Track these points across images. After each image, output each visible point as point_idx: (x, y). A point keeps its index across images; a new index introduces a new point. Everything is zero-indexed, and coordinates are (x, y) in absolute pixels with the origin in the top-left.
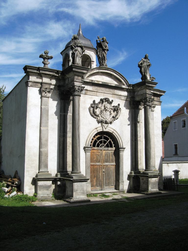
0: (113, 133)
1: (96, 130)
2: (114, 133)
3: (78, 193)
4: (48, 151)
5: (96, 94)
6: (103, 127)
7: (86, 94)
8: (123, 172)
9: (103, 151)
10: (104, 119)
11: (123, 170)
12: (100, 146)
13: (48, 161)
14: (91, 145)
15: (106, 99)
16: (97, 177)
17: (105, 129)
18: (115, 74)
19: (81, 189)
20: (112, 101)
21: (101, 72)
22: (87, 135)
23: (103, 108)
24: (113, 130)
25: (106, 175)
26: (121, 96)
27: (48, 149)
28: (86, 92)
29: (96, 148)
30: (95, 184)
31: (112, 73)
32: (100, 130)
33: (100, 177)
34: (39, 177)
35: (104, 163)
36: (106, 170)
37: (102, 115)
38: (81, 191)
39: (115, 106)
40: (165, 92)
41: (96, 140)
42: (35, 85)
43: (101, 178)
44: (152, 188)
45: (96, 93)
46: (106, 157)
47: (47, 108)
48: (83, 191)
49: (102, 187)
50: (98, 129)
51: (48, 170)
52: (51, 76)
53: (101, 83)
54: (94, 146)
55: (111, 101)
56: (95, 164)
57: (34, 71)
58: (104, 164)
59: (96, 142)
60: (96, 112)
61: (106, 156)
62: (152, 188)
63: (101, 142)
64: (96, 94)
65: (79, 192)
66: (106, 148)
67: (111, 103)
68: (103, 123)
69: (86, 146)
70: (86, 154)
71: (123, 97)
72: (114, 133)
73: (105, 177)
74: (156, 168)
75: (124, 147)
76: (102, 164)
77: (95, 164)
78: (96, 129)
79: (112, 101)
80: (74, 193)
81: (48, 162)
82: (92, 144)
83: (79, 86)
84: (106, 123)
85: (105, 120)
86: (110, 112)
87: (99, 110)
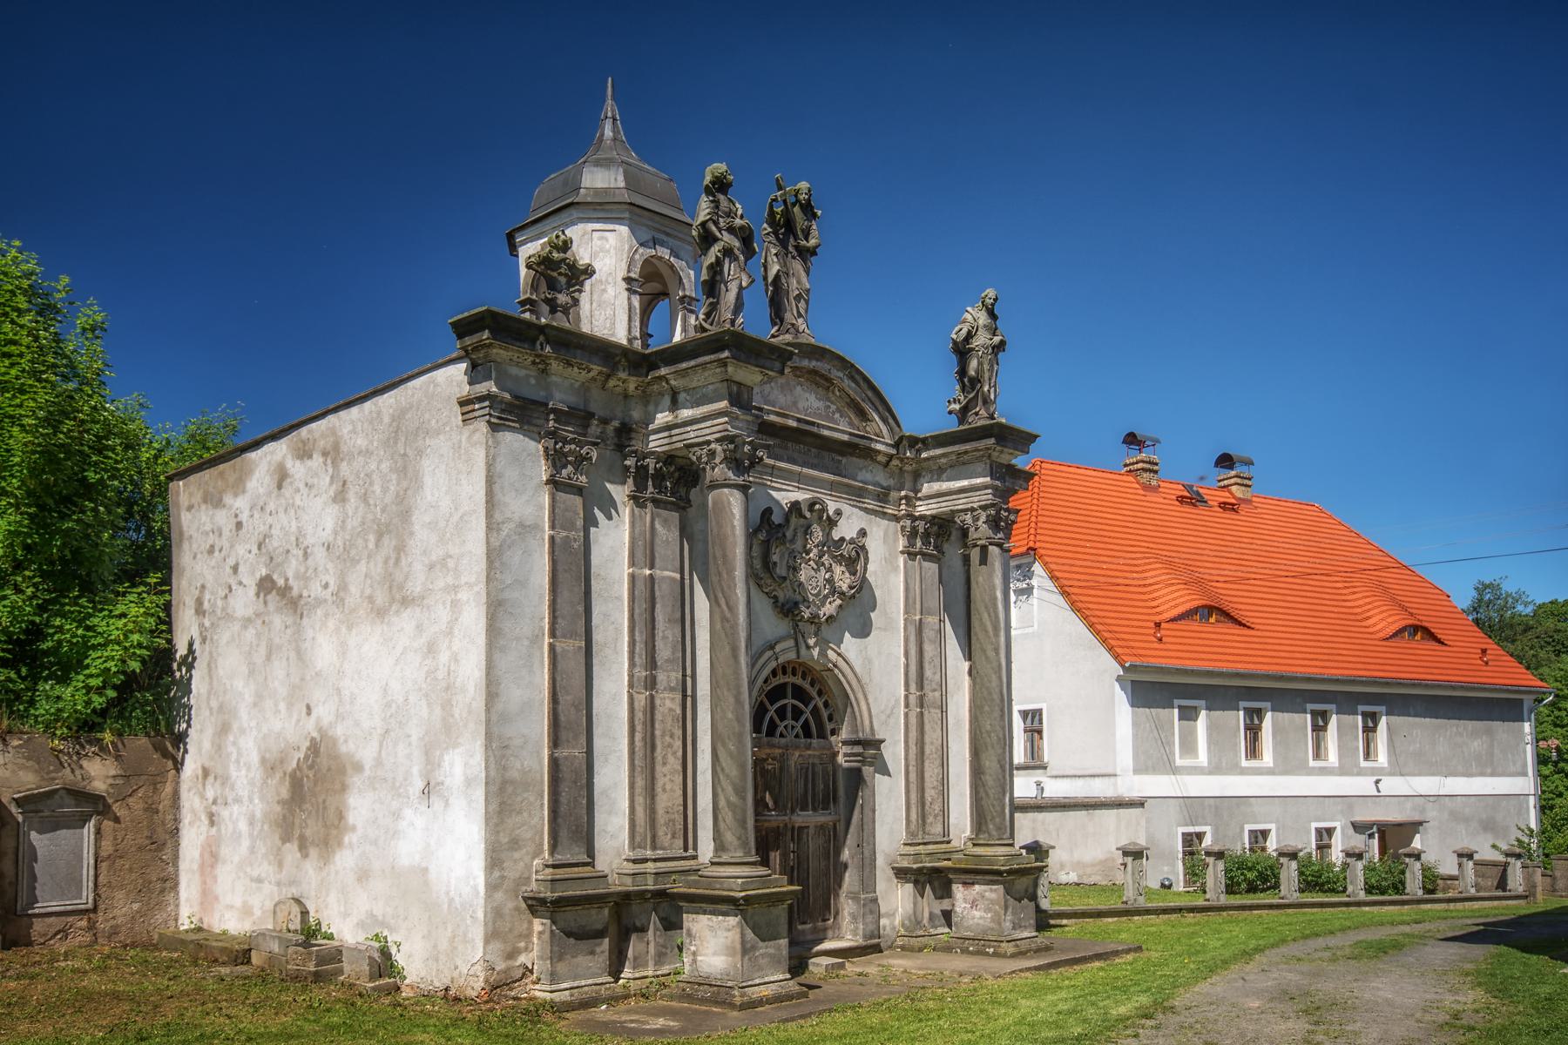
1: (769, 653)
20: (839, 513)
79: (839, 513)
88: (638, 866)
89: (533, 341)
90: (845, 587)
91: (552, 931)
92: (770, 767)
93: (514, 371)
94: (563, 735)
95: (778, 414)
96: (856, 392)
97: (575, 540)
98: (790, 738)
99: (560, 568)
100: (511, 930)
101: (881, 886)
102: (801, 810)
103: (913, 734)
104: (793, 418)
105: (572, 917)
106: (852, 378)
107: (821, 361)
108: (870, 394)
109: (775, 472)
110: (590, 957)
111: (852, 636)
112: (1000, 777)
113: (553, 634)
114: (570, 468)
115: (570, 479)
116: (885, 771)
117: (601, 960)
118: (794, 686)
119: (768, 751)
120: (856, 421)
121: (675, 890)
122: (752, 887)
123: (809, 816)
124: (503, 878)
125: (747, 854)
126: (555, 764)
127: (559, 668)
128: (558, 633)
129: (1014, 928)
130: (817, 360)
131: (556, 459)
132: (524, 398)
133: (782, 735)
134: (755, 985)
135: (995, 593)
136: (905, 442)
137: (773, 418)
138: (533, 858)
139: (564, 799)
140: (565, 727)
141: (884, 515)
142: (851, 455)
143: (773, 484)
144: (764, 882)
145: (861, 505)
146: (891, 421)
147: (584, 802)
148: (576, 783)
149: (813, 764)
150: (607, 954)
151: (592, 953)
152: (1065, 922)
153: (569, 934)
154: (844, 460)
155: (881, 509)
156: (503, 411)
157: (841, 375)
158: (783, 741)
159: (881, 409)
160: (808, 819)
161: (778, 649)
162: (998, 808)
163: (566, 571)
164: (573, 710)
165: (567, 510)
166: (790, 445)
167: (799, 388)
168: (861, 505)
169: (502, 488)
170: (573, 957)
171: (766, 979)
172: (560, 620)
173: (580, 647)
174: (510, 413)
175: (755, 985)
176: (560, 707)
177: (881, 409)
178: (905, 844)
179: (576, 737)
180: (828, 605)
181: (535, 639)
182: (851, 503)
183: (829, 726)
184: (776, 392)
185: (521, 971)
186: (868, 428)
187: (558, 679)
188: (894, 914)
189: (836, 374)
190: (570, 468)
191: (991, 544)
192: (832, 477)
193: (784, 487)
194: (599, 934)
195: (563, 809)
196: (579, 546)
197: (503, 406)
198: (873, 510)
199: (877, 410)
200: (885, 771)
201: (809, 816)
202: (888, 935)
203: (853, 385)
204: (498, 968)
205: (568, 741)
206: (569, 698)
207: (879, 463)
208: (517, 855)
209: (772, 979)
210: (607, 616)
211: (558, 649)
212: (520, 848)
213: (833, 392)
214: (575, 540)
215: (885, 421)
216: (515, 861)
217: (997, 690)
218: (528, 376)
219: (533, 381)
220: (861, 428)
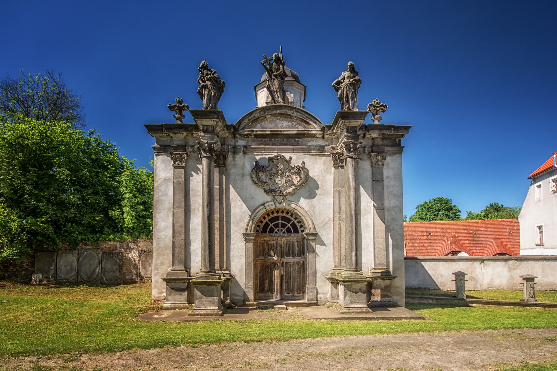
0: (295, 211)
1: (263, 207)
20: (291, 158)
44: (351, 302)
54: (264, 231)
55: (288, 159)
79: (291, 158)
82: (260, 229)
88: (334, 271)
89: (162, 130)
90: (296, 182)
91: (167, 288)
92: (271, 243)
93: (162, 139)
94: (176, 235)
95: (261, 131)
96: (300, 116)
97: (181, 181)
98: (279, 233)
99: (176, 189)
100: (160, 286)
101: (318, 284)
102: (287, 257)
103: (338, 230)
104: (268, 131)
105: (173, 284)
106: (297, 112)
107: (282, 109)
108: (306, 115)
109: (265, 149)
110: (180, 296)
111: (305, 199)
112: (350, 245)
113: (173, 208)
114: (178, 162)
115: (178, 164)
116: (323, 244)
117: (184, 297)
118: (282, 217)
119: (270, 238)
120: (307, 126)
121: (61, 280)
122: (201, 279)
123: (291, 259)
124: (158, 273)
125: (206, 269)
126: (174, 242)
127: (175, 217)
128: (174, 207)
129: (351, 302)
130: (280, 110)
131: (174, 160)
132: (163, 146)
133: (276, 233)
134: (201, 309)
135: (349, 176)
136: (326, 128)
137: (258, 133)
138: (169, 268)
139: (176, 252)
140: (177, 233)
141: (324, 155)
142: (304, 137)
143: (265, 153)
144: (206, 278)
145: (310, 153)
146: (318, 122)
147: (184, 253)
148: (180, 248)
149: (293, 242)
150: (187, 295)
151: (181, 295)
152: (474, 305)
153: (173, 289)
154: (301, 140)
155: (321, 153)
156: (158, 150)
157: (293, 112)
158: (276, 235)
159: (312, 119)
160: (292, 260)
161: (266, 205)
162: (349, 257)
163: (178, 190)
164: (180, 228)
165: (178, 173)
166: (273, 139)
167: (278, 121)
168: (311, 154)
169: (159, 171)
170: (174, 295)
171: (206, 308)
172: (175, 204)
173: (183, 211)
174: (160, 150)
175: (201, 309)
176: (175, 227)
177: (312, 119)
178: (333, 269)
179: (181, 235)
180: (289, 189)
181: (169, 209)
182: (305, 153)
183: (300, 229)
184: (267, 124)
185: (164, 298)
186: (311, 127)
187: (175, 219)
188: (326, 293)
189: (289, 112)
190: (178, 162)
191: (348, 158)
192: (293, 147)
193: (270, 153)
194: (183, 290)
195: (176, 255)
196: (183, 183)
197: (158, 149)
198: (317, 154)
199: (311, 120)
200: (323, 244)
201: (291, 259)
202: (323, 300)
203: (299, 114)
204: (156, 296)
205: (178, 236)
206: (178, 225)
207: (319, 138)
208: (163, 267)
209: (209, 308)
210: (195, 201)
211: (175, 212)
212: (164, 265)
213: (293, 118)
214: (181, 181)
215: (316, 123)
216: (162, 268)
217: (349, 212)
218: (167, 140)
219: (169, 140)
220: (309, 128)
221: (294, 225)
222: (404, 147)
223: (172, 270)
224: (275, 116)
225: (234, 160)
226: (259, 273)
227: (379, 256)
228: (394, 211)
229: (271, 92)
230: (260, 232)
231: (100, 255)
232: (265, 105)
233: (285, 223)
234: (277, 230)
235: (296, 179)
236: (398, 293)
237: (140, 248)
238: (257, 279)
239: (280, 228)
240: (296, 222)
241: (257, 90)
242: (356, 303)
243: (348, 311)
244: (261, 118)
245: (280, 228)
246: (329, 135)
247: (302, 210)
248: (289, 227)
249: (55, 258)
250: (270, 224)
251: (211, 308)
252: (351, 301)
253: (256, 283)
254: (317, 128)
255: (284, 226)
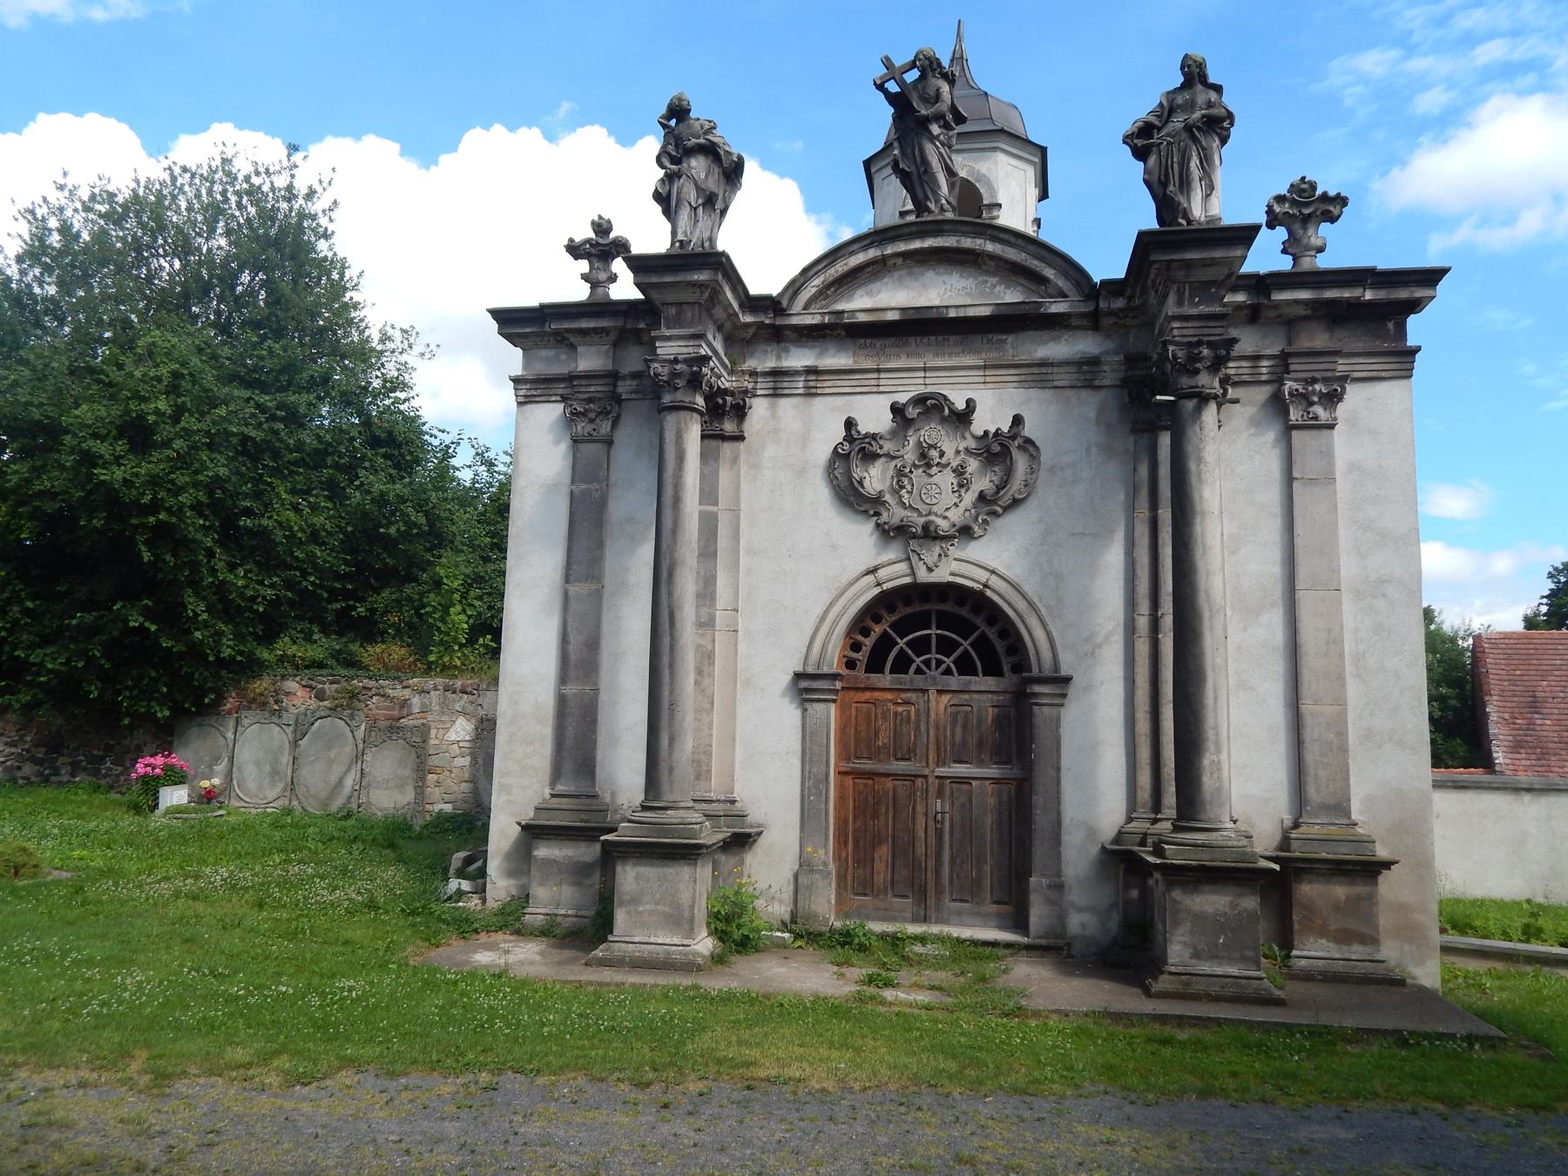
0: (988, 593)
1: (870, 578)
2: (994, 591)
3: (641, 912)
4: (596, 699)
5: (873, 382)
6: (914, 558)
7: (813, 391)
8: (1059, 824)
9: (933, 695)
10: (915, 515)
11: (1059, 813)
12: (914, 667)
13: (595, 743)
14: (851, 664)
15: (920, 400)
16: (893, 842)
17: (930, 570)
18: (990, 247)
19: (658, 896)
20: (970, 404)
21: (905, 255)
22: (819, 610)
23: (910, 455)
24: (982, 576)
25: (956, 836)
26: (1052, 365)
27: (596, 684)
28: (811, 384)
29: (886, 679)
30: (881, 877)
31: (967, 243)
32: (896, 574)
33: (917, 845)
34: (1124, 830)
35: (940, 762)
36: (957, 804)
37: (906, 496)
38: (661, 908)
39: (993, 430)
40: (1432, 277)
41: (885, 634)
42: (546, 392)
43: (920, 850)
44: (1196, 955)
45: (875, 376)
46: (959, 729)
47: (597, 490)
48: (677, 906)
49: (931, 901)
50: (882, 573)
51: (593, 785)
52: (613, 336)
53: (892, 316)
54: (875, 665)
55: (960, 405)
56: (882, 771)
57: (515, 328)
58: (942, 771)
59: (885, 643)
60: (861, 483)
61: (954, 722)
62: (1196, 955)
63: (921, 646)
64: (873, 382)
65: (651, 913)
66: (955, 681)
67: (962, 418)
68: (914, 536)
69: (811, 670)
70: (805, 710)
71: (1061, 370)
72: (994, 591)
73: (951, 849)
74: (1355, 816)
75: (1063, 673)
76: (926, 772)
77: (881, 768)
78: (873, 571)
79: (970, 404)
80: (620, 917)
81: (595, 748)
82: (862, 657)
83: (672, 357)
84: (930, 534)
85: (922, 520)
86: (959, 472)
87: (884, 472)
133: (919, 671)
171: (652, 940)
172: (574, 567)
221: (982, 645)
222: (1418, 349)
223: (553, 796)
224: (918, 258)
225: (773, 415)
226: (854, 821)
227: (1321, 773)
228: (1384, 595)
229: (180, 261)
230: (861, 666)
231: (360, 733)
232: (896, 220)
233: (954, 636)
234: (923, 662)
235: (875, 478)
236: (1411, 933)
237: (482, 712)
238: (846, 843)
239: (934, 656)
240: (991, 634)
241: (873, 171)
242: (1217, 957)
243: (1180, 988)
244: (868, 270)
245: (934, 656)
246: (1118, 317)
247: (849, 594)
248: (966, 651)
249: (230, 735)
250: (899, 640)
251: (668, 941)
252: (1195, 948)
253: (844, 855)
254: (1069, 294)
255: (946, 647)
